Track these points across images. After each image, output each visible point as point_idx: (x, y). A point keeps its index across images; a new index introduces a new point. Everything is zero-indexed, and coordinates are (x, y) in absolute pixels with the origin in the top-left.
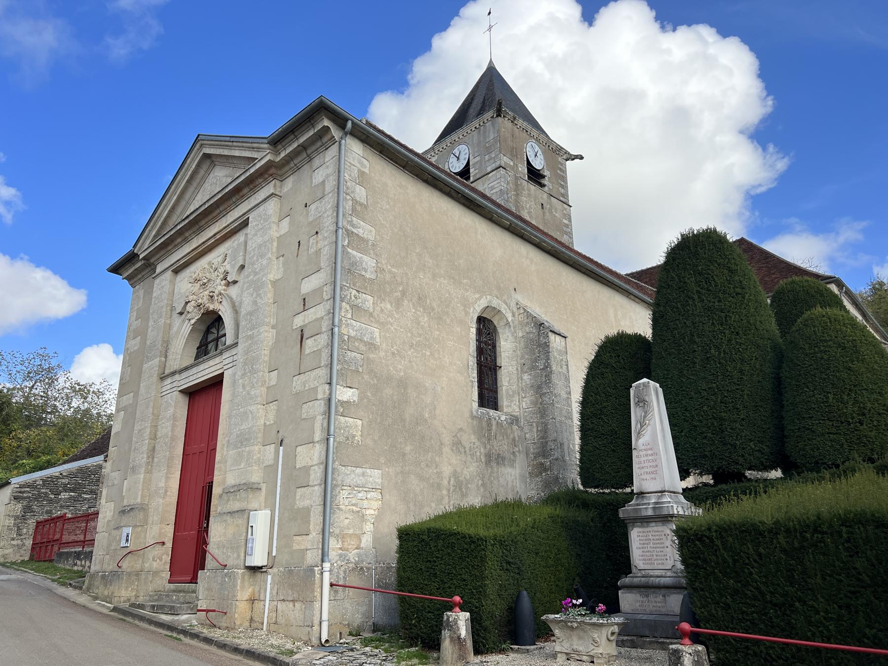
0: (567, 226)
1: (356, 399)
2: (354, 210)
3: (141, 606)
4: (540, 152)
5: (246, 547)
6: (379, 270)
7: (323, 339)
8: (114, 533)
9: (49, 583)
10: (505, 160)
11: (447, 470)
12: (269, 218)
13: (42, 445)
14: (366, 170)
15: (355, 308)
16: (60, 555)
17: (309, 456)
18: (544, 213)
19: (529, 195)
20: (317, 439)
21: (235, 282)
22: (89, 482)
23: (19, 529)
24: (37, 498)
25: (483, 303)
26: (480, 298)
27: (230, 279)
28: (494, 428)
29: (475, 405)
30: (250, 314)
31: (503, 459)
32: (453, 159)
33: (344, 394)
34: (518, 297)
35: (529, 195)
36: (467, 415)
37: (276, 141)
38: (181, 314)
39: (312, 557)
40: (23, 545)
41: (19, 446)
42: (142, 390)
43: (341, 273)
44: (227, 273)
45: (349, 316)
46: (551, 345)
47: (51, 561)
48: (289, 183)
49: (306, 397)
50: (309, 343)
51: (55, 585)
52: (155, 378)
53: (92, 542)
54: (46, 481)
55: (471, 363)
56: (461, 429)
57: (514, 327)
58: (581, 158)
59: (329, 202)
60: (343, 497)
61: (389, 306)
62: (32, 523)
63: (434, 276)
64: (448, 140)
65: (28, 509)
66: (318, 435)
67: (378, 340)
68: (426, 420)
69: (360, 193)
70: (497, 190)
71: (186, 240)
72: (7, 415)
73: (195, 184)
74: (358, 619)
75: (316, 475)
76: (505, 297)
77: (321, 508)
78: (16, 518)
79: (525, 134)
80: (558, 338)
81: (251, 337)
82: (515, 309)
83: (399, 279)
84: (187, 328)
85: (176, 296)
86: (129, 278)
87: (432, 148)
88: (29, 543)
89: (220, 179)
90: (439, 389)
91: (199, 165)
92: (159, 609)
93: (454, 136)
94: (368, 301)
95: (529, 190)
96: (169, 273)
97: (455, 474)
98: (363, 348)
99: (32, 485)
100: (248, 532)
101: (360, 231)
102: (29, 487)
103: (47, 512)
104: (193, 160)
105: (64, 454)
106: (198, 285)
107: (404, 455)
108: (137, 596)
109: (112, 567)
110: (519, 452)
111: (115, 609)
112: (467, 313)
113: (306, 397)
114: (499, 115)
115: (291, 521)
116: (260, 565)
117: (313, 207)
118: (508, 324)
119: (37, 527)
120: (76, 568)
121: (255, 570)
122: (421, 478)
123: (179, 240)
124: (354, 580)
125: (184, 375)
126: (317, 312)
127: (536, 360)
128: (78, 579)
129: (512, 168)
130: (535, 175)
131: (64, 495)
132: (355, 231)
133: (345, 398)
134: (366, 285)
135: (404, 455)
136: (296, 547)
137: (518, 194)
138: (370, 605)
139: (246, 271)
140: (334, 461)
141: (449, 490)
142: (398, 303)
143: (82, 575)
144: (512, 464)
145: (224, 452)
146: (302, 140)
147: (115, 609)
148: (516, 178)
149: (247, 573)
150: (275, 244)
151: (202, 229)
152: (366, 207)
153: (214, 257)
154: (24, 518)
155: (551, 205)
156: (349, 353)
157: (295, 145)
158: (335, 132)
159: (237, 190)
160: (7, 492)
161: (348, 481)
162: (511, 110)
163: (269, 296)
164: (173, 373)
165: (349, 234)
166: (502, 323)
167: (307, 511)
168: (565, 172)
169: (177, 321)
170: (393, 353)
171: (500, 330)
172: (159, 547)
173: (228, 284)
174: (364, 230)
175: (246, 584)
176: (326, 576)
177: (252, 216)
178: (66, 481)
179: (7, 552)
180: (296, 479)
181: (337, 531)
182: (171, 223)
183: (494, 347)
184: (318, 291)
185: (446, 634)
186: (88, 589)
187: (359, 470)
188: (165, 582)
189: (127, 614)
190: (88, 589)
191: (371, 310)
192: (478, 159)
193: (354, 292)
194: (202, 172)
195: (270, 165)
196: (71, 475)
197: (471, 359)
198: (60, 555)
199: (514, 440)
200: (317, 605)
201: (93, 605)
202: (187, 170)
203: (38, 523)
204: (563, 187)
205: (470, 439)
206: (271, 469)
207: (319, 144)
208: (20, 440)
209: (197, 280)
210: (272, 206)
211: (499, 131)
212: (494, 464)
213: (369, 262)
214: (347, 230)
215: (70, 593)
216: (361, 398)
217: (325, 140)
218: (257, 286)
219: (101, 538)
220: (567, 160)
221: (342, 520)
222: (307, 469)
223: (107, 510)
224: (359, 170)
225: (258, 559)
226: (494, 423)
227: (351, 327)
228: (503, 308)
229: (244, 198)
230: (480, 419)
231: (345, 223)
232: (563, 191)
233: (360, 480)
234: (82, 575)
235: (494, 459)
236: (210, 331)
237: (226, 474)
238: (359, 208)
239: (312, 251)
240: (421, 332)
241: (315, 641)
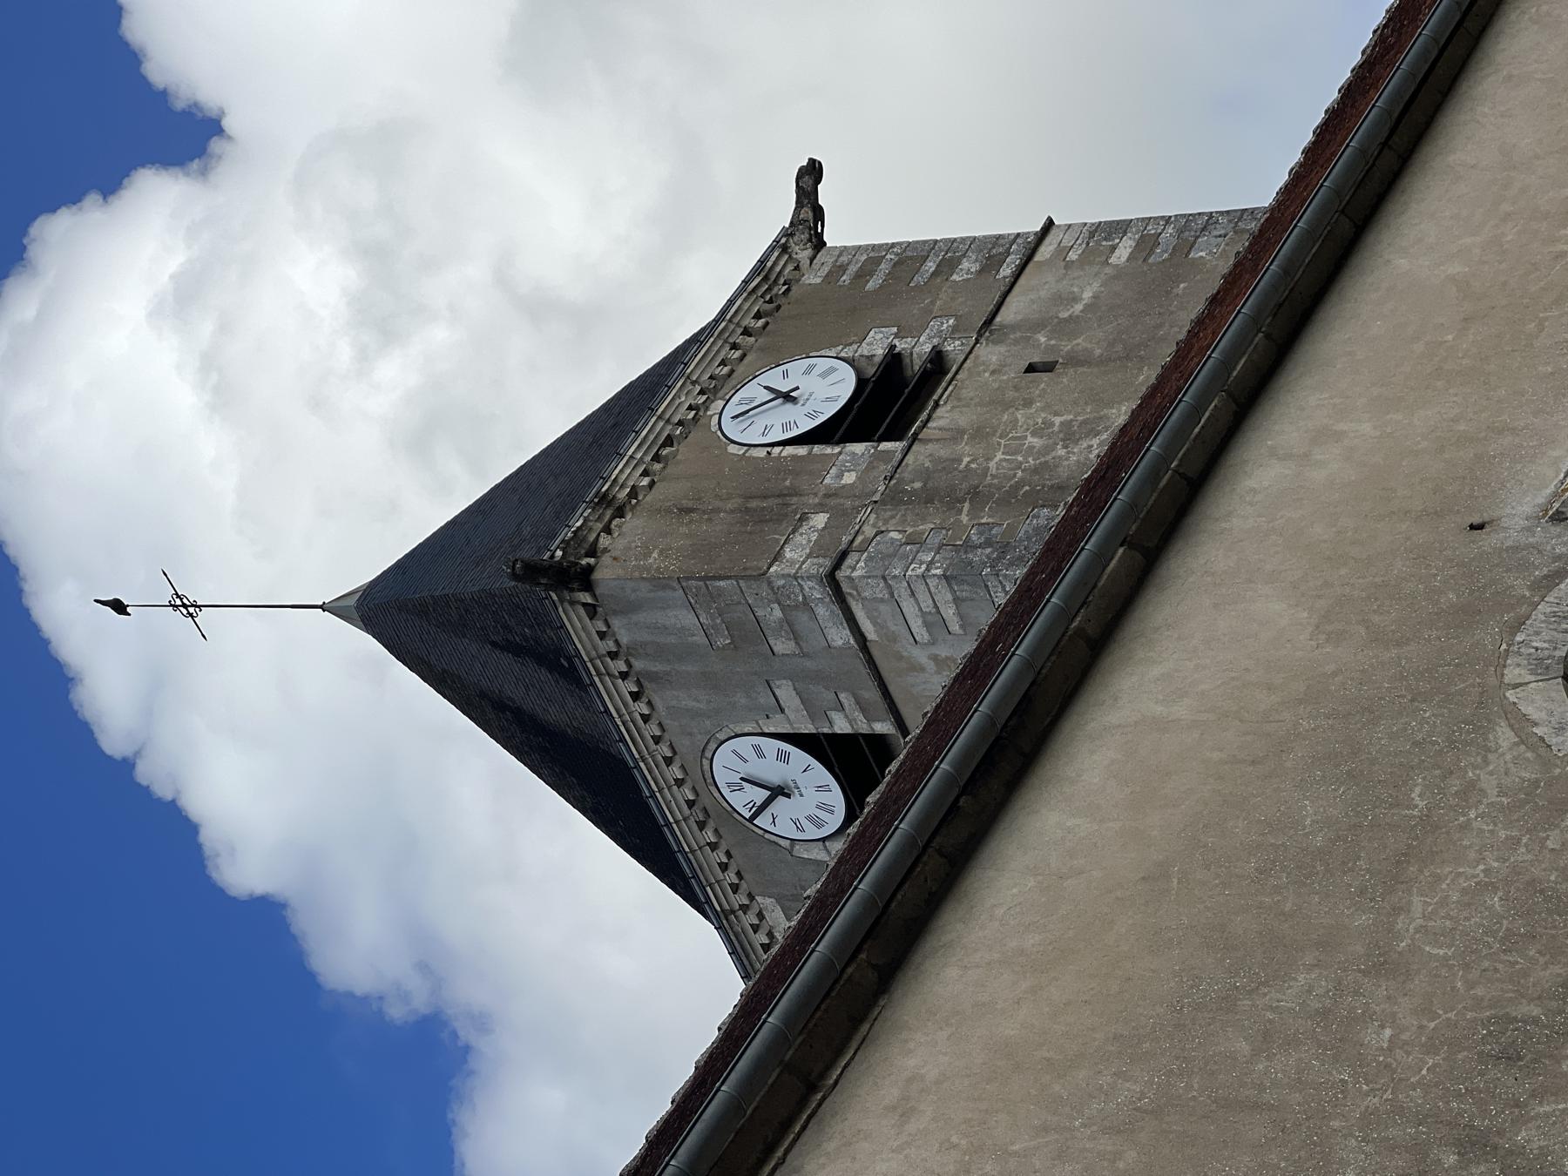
0: (1147, 244)
10: (799, 553)
19: (980, 434)
32: (783, 820)
58: (812, 173)
64: (687, 837)
70: (944, 596)
76: (1520, 586)
79: (683, 451)
93: (671, 805)
95: (956, 434)
114: (585, 579)
129: (841, 517)
130: (888, 402)
148: (894, 498)
155: (1039, 326)
192: (786, 692)
211: (659, 582)
220: (819, 244)
232: (969, 266)
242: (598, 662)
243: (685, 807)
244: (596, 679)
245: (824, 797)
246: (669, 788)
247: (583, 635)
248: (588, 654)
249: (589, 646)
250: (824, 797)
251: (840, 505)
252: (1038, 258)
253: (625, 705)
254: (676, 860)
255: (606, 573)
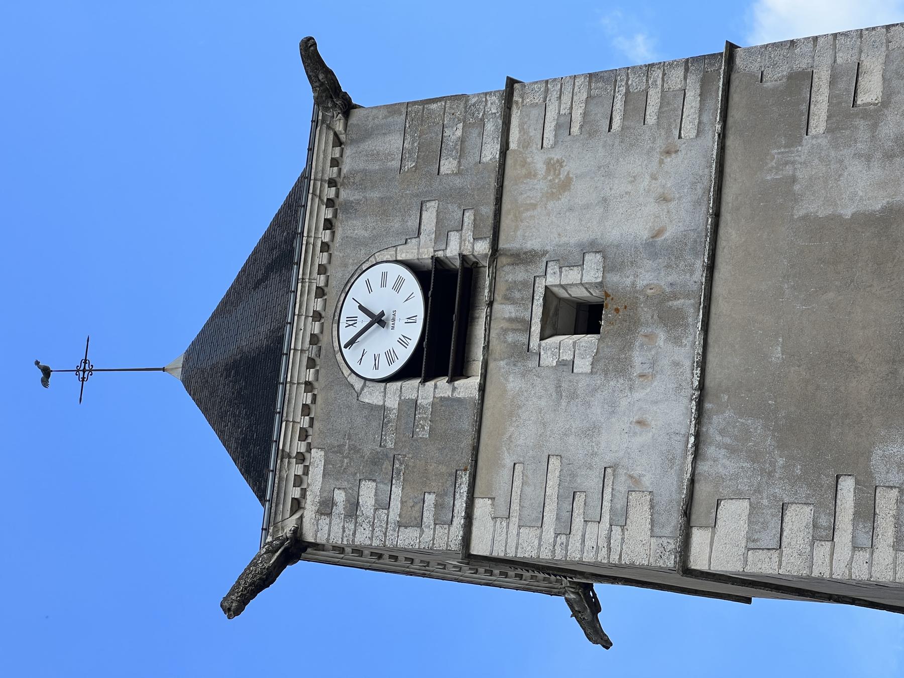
58: (309, 52)
242: (319, 183)
243: (308, 339)
244: (310, 196)
245: (376, 283)
246: (307, 317)
247: (322, 156)
248: (316, 173)
249: (320, 168)
250: (376, 283)
252: (513, 146)
253: (317, 229)
254: (273, 420)
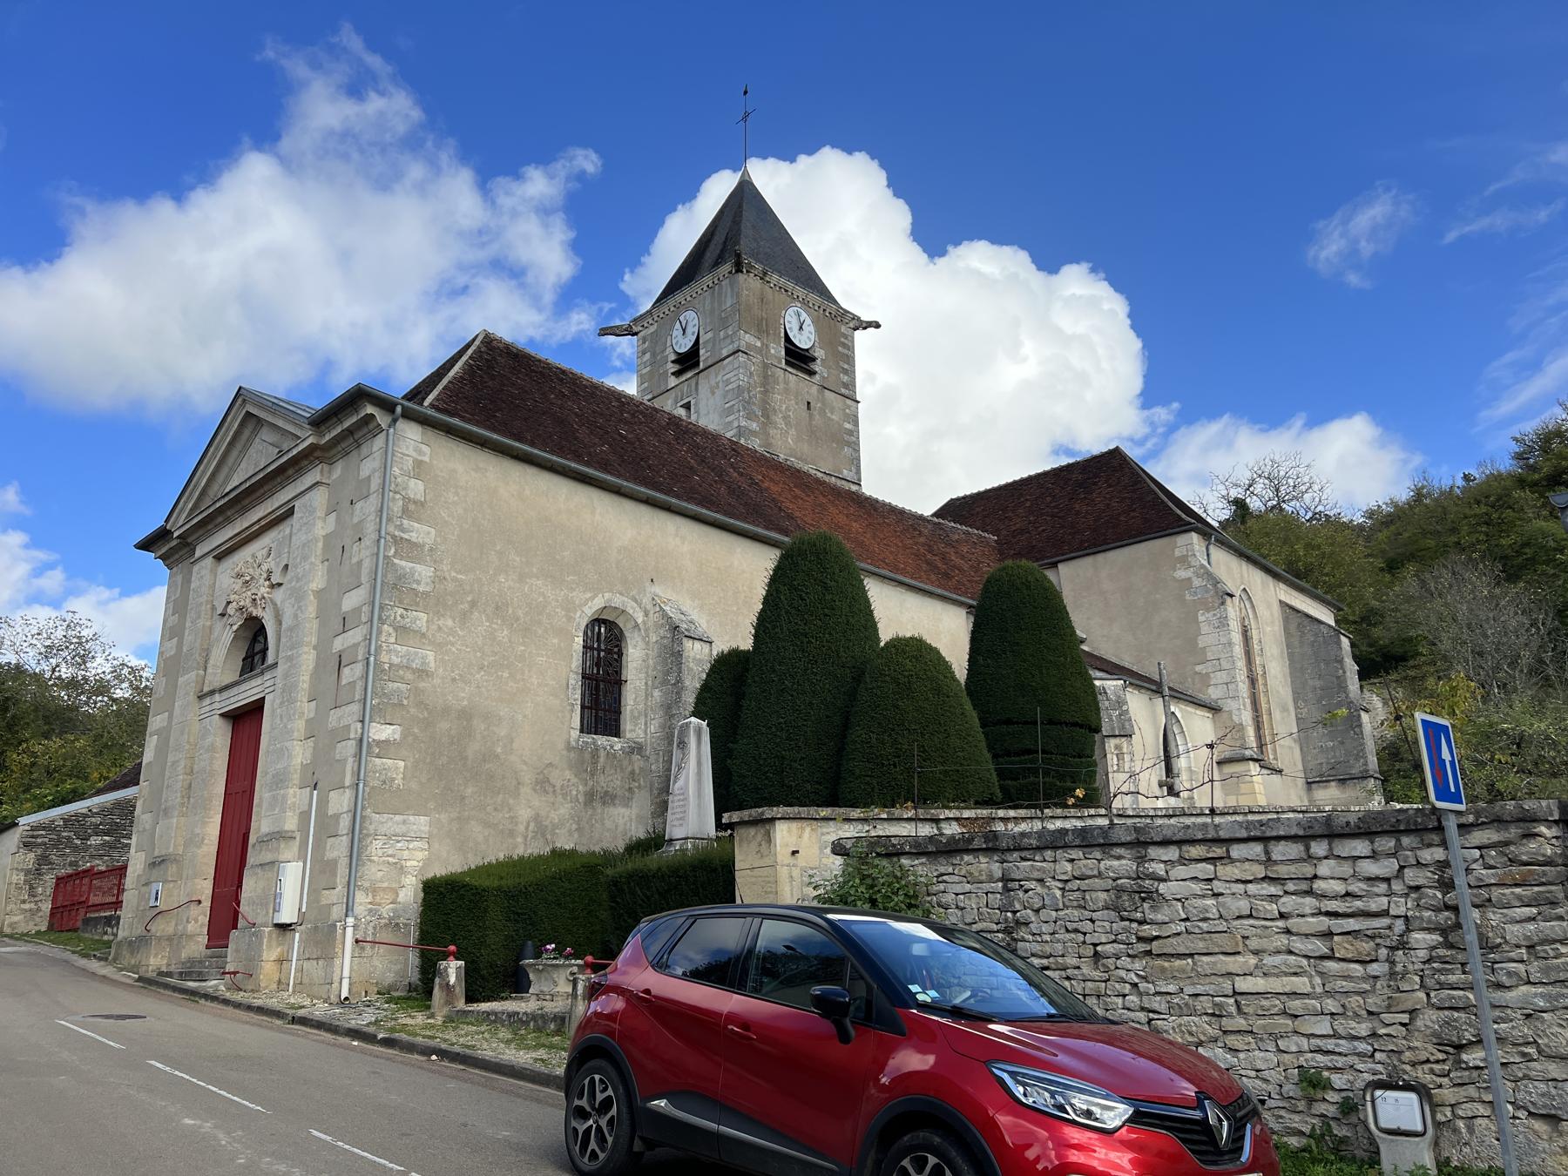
0: (850, 433)
1: (397, 736)
2: (405, 510)
3: (169, 974)
4: (808, 321)
5: (275, 902)
6: (439, 579)
7: (358, 669)
8: (144, 889)
9: (68, 955)
10: (748, 339)
11: (524, 814)
12: (315, 509)
13: (68, 763)
14: (426, 459)
15: (402, 630)
16: (87, 922)
17: (340, 802)
18: (811, 416)
19: (787, 390)
20: (347, 783)
21: (280, 585)
22: (120, 822)
23: (31, 888)
24: (57, 844)
25: (598, 603)
26: (592, 599)
27: (274, 580)
28: (602, 760)
29: (575, 733)
30: (291, 629)
31: (613, 797)
32: (677, 331)
33: (381, 732)
34: (657, 589)
35: (787, 390)
36: (561, 745)
37: (321, 421)
38: (223, 615)
39: (337, 912)
40: (39, 910)
41: (33, 764)
42: (177, 711)
43: (391, 588)
44: (270, 572)
45: (392, 640)
46: (685, 654)
47: (76, 930)
48: (338, 470)
49: (340, 735)
50: (346, 671)
51: (75, 957)
52: (192, 697)
53: (118, 904)
54: (68, 821)
55: (572, 682)
56: (551, 764)
57: (646, 630)
58: (877, 326)
59: (374, 501)
60: (376, 848)
61: (450, 623)
62: (49, 879)
63: (522, 578)
64: (671, 302)
65: (43, 860)
66: (348, 781)
67: (432, 665)
68: (497, 756)
69: (416, 488)
70: (734, 386)
71: (229, 521)
72: (13, 717)
73: (239, 446)
74: (390, 978)
75: (345, 822)
76: (634, 593)
77: (346, 860)
78: (28, 872)
79: (783, 296)
80: (698, 645)
81: (290, 659)
82: (649, 607)
83: (468, 588)
84: (227, 636)
85: (217, 593)
86: (163, 558)
87: (649, 312)
88: (47, 907)
89: (259, 456)
90: (520, 717)
91: (242, 425)
92: (184, 975)
93: (679, 297)
94: (420, 619)
95: (787, 383)
96: (209, 560)
97: (537, 818)
98: (409, 676)
99: (48, 827)
100: (285, 888)
101: (413, 537)
102: (44, 829)
103: (71, 864)
104: (234, 418)
105: (102, 778)
106: (240, 582)
107: (463, 798)
108: (168, 965)
109: (140, 931)
110: (639, 787)
111: (140, 979)
112: (570, 619)
113: (340, 735)
114: (739, 271)
115: (321, 874)
116: (288, 921)
117: (358, 506)
118: (637, 626)
119: (57, 885)
120: (106, 938)
121: (284, 928)
122: (487, 825)
123: (220, 519)
124: (384, 936)
125: (225, 694)
126: (355, 636)
127: (668, 673)
128: (102, 950)
129: (759, 351)
130: (799, 358)
131: (95, 841)
132: (405, 536)
133: (383, 737)
134: (416, 600)
135: (463, 798)
136: (324, 902)
137: (766, 391)
138: (406, 964)
139: (290, 573)
140: (363, 808)
141: (526, 838)
142: (464, 617)
143: (108, 944)
144: (627, 803)
145: (262, 794)
146: (347, 424)
147: (140, 979)
148: (766, 366)
149: (276, 932)
150: (320, 544)
151: (245, 510)
152: (422, 504)
153: (257, 548)
154: (38, 873)
155: (824, 403)
156: (390, 684)
157: (339, 429)
158: (382, 419)
159: (281, 470)
160: (13, 838)
161: (383, 830)
162: (758, 261)
163: (311, 610)
164: (212, 692)
165: (397, 541)
166: (629, 626)
167: (335, 862)
168: (851, 348)
169: (219, 625)
170: (454, 680)
171: (627, 634)
172: (193, 906)
173: (272, 586)
174: (419, 532)
175: (274, 943)
176: (349, 931)
177: (297, 504)
178: (97, 820)
179: (16, 919)
180: (327, 828)
181: (367, 884)
182: (215, 491)
183: (620, 654)
184: (357, 610)
185: (437, 980)
186: (115, 960)
187: (398, 818)
188: (202, 948)
189: (152, 983)
190: (115, 960)
191: (424, 630)
192: (710, 335)
193: (400, 611)
194: (247, 433)
195: (313, 448)
196: (103, 811)
197: (572, 676)
198: (87, 922)
199: (633, 772)
200: (337, 962)
201: (118, 977)
202: (228, 430)
203: (58, 879)
204: (846, 372)
205: (562, 775)
206: (304, 816)
207: (365, 430)
208: (34, 754)
209: (240, 576)
210: (319, 498)
211: (738, 295)
212: (598, 805)
213: (423, 572)
214: (394, 537)
215: (94, 965)
216: (404, 736)
217: (371, 426)
218: (298, 596)
219: (129, 898)
220: (856, 329)
221: (373, 872)
222: (337, 817)
223: (136, 863)
224: (415, 461)
225: (287, 916)
226: (602, 753)
227: (394, 652)
228: (632, 607)
229: (290, 480)
230: (581, 750)
231: (391, 529)
232: (845, 379)
233: (401, 829)
234: (108, 944)
235: (597, 798)
236: (254, 645)
237: (261, 825)
238: (412, 507)
239: (354, 560)
240: (497, 649)
241: (334, 999)
251: (763, 351)
255: (741, 277)
